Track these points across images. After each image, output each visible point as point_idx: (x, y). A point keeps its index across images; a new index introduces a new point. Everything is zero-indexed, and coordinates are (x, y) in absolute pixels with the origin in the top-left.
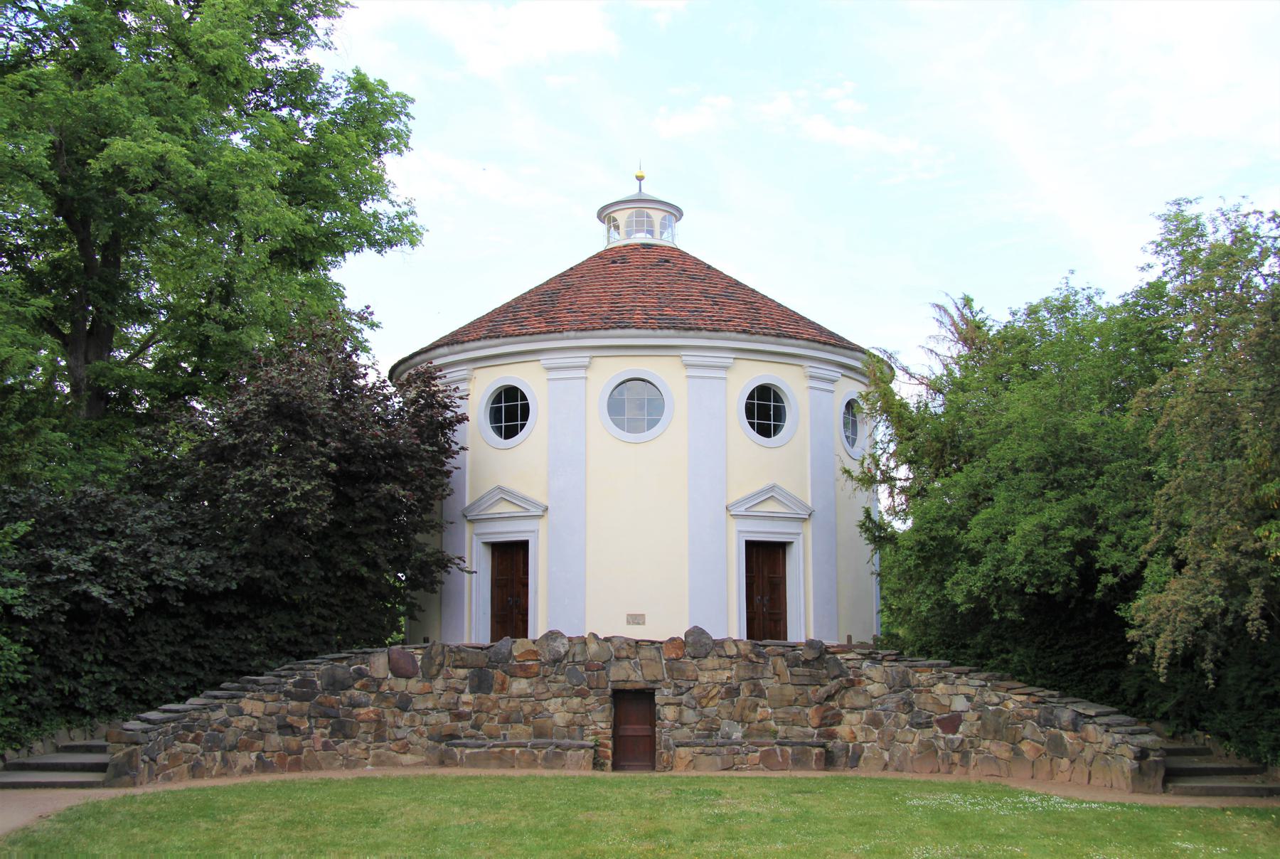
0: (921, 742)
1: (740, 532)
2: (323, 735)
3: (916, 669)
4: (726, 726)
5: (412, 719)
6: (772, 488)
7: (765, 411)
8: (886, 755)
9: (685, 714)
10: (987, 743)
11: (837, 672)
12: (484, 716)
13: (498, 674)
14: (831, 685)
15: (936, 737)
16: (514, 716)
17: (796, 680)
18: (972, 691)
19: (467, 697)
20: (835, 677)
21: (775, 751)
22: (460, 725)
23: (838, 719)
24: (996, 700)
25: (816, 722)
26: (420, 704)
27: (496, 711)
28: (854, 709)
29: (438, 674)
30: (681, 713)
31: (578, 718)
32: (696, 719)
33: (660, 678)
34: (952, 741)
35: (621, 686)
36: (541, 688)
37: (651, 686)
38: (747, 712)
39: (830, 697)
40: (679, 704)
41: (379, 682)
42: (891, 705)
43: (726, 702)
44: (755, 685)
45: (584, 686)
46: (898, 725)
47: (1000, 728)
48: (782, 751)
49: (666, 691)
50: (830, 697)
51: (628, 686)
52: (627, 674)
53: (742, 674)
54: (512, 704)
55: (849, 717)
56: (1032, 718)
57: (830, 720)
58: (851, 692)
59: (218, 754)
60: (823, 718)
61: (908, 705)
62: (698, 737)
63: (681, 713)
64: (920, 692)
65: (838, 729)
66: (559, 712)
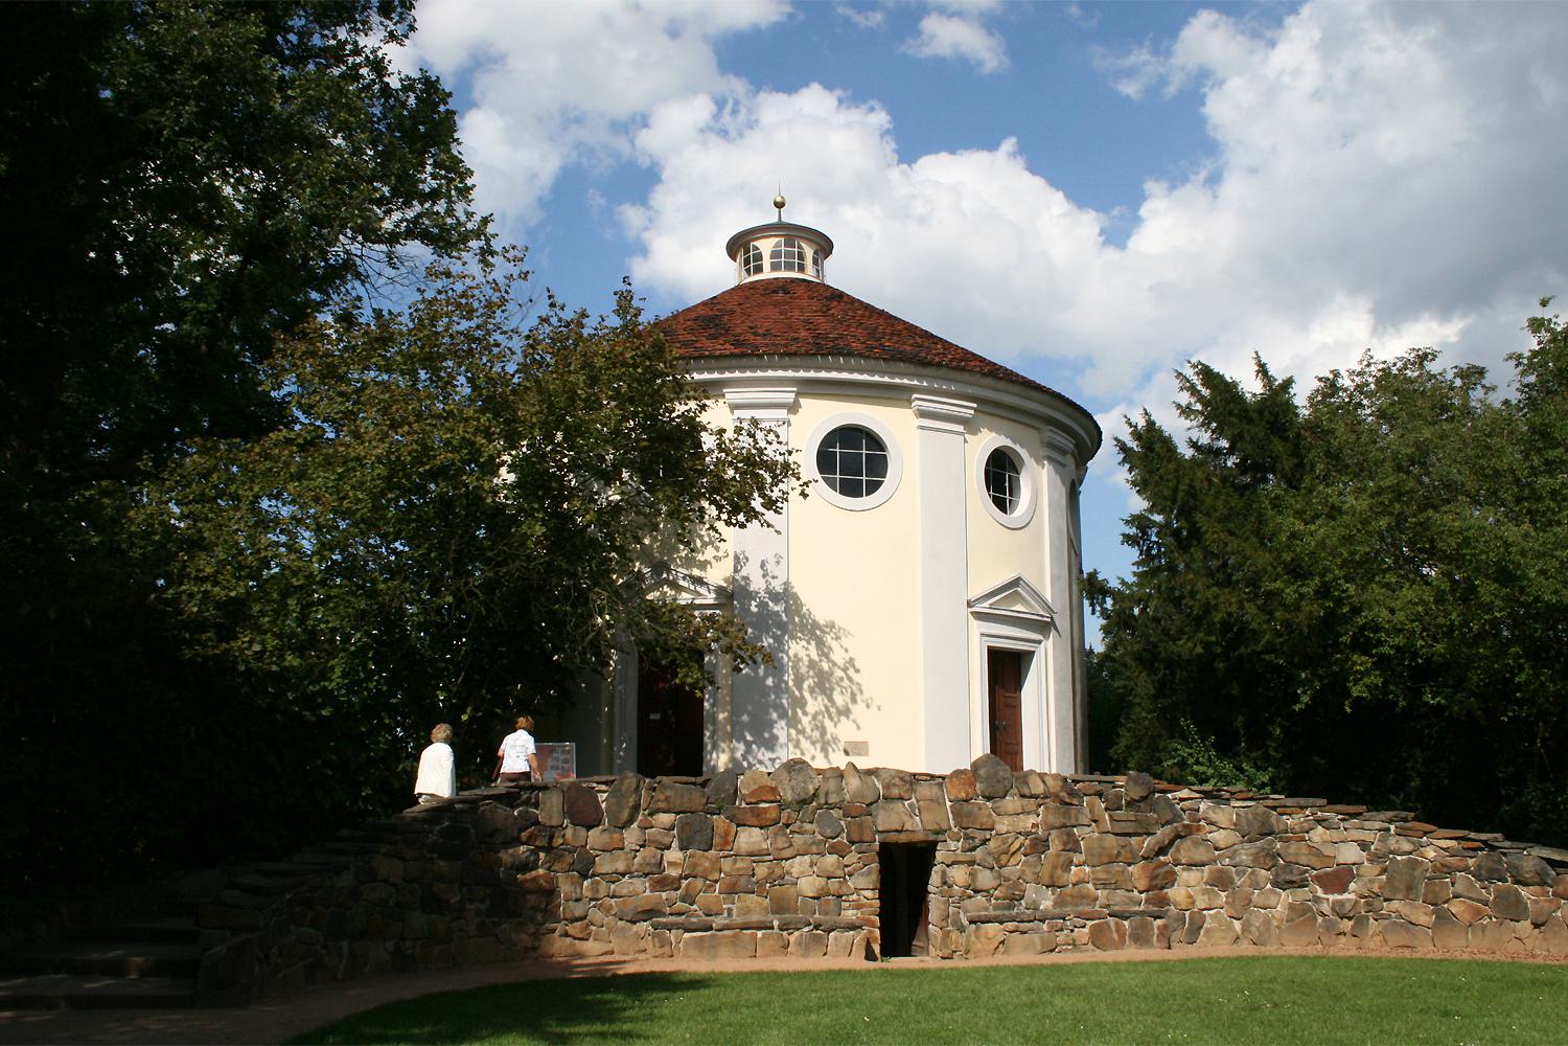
0: (1291, 907)
1: (982, 635)
2: (478, 913)
3: (1281, 810)
4: (1031, 891)
5: (595, 887)
6: (1016, 582)
7: (1000, 475)
8: (1237, 925)
9: (980, 876)
10: (1395, 905)
11: (1169, 816)
12: (699, 883)
13: (719, 821)
14: (1162, 833)
15: (1317, 900)
16: (743, 881)
17: (1119, 828)
18: (1367, 836)
19: (674, 855)
20: (1167, 823)
21: (1108, 924)
22: (664, 895)
23: (1170, 879)
24: (1407, 847)
25: (1142, 884)
26: (604, 865)
27: (715, 876)
28: (1191, 865)
29: (631, 821)
30: (973, 875)
31: (833, 884)
32: (995, 884)
33: (944, 826)
34: (1341, 903)
35: (893, 838)
36: (781, 842)
37: (932, 837)
38: (1059, 872)
39: (1162, 850)
40: (972, 863)
41: (552, 831)
42: (1244, 857)
43: (1031, 859)
44: (1068, 834)
45: (843, 838)
46: (1255, 885)
47: (1405, 881)
48: (1117, 924)
49: (952, 845)
50: (1162, 850)
51: (903, 838)
52: (905, 820)
53: (1051, 819)
54: (740, 864)
55: (1187, 877)
56: (1466, 869)
57: (1160, 882)
58: (1187, 843)
59: (345, 944)
60: (1153, 878)
61: (1269, 858)
62: (996, 908)
63: (973, 875)
64: (1287, 841)
65: (1170, 892)
66: (805, 876)
